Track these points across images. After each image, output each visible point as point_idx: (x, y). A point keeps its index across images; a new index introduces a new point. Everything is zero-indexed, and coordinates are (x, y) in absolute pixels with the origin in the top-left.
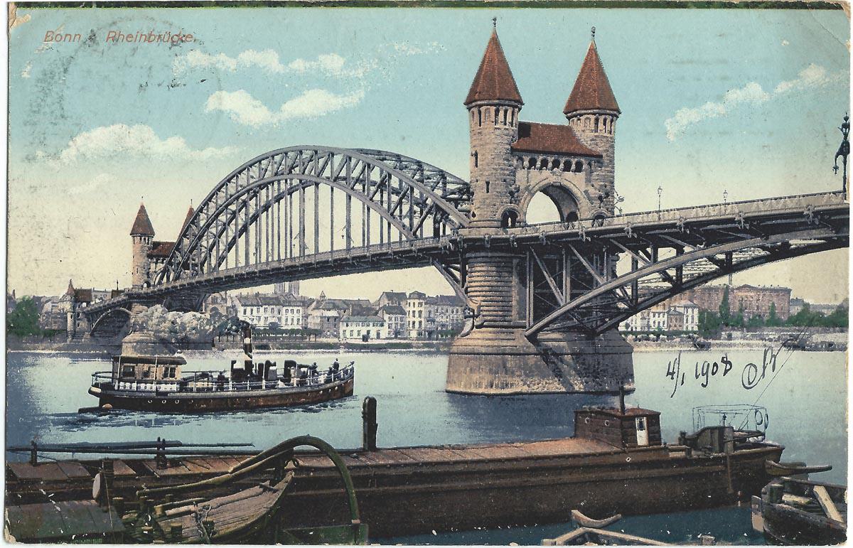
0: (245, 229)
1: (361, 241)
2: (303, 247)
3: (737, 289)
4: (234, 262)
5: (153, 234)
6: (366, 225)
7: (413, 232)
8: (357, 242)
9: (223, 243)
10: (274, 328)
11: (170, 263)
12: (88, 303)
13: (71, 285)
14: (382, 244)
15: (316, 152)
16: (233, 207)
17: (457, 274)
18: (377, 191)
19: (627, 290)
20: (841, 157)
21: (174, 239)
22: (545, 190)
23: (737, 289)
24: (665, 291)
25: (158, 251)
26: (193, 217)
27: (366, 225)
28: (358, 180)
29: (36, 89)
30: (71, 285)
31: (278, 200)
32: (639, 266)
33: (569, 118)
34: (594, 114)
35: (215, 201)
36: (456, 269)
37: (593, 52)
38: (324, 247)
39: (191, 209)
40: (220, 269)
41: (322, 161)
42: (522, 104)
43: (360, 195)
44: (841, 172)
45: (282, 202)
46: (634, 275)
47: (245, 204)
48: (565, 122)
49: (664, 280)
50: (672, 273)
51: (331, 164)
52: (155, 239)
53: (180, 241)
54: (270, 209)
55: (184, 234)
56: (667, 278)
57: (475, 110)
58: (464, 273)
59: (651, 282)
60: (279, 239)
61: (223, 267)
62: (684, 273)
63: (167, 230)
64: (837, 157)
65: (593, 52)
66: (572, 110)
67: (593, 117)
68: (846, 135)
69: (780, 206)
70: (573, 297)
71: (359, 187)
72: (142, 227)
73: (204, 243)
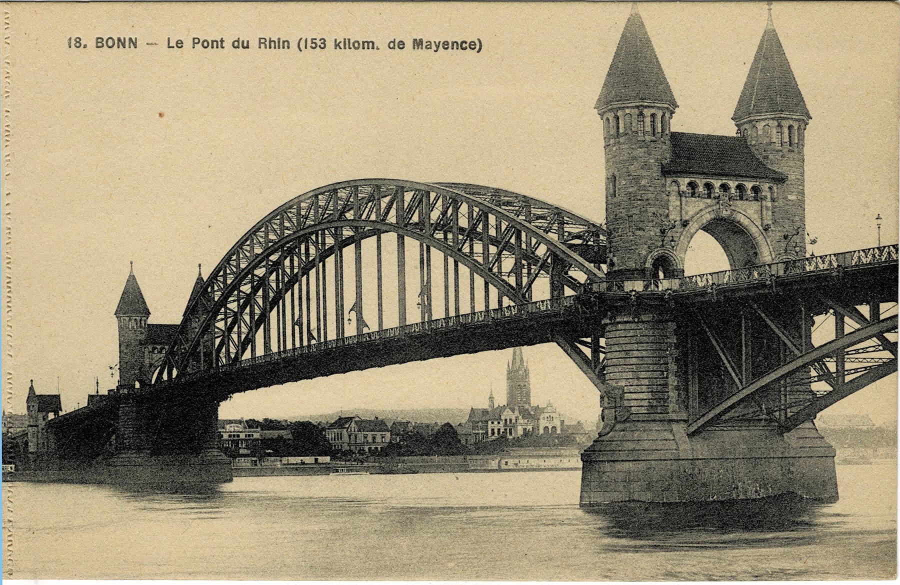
0: (264, 319)
1: (508, 473)
2: (361, 322)
5: (148, 313)
7: (520, 294)
11: (171, 353)
12: (56, 413)
13: (31, 389)
15: (378, 187)
16: (260, 272)
17: (587, 351)
18: (467, 239)
19: (502, 224)
26: (202, 289)
28: (437, 227)
29: (673, 222)
30: (31, 389)
31: (305, 271)
32: (847, 330)
36: (585, 344)
38: (391, 321)
39: (200, 279)
40: (244, 358)
41: (385, 202)
43: (443, 246)
45: (313, 272)
46: (840, 343)
47: (278, 264)
52: (152, 320)
54: (296, 286)
57: (611, 116)
58: (596, 350)
59: (859, 353)
61: (247, 355)
70: (757, 374)
71: (439, 235)
73: (221, 325)
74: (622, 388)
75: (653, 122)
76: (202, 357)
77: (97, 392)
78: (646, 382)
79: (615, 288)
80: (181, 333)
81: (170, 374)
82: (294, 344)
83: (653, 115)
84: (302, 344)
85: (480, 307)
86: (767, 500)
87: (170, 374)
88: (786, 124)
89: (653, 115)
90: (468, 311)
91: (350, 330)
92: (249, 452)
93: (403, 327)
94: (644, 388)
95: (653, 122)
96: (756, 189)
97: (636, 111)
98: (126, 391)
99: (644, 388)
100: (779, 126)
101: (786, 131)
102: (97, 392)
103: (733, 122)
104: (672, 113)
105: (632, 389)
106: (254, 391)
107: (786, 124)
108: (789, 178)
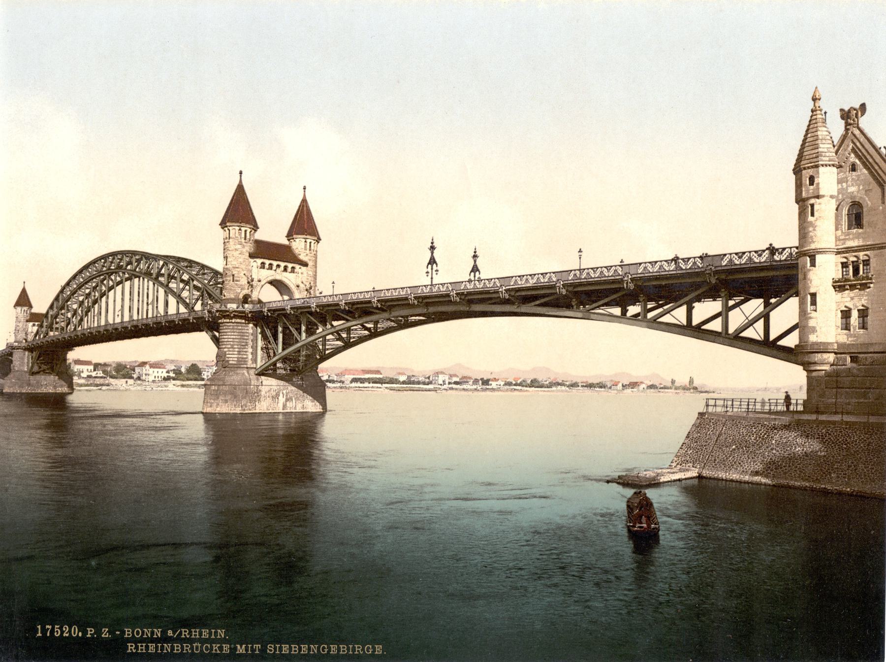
2: (107, 320)
6: (167, 304)
8: (126, 319)
14: (153, 317)
25: (34, 318)
27: (167, 304)
33: (289, 240)
34: (250, 228)
37: (304, 201)
44: (430, 275)
50: (344, 335)
52: (33, 311)
53: (48, 312)
55: (51, 307)
56: (340, 338)
60: (138, 309)
62: (379, 326)
63: (41, 305)
65: (304, 201)
66: (290, 236)
67: (238, 228)
69: (397, 294)
72: (23, 300)
74: (226, 352)
76: (679, 281)
78: (236, 350)
79: (223, 306)
83: (246, 231)
86: (223, 420)
88: (308, 241)
89: (246, 231)
91: (118, 320)
92: (352, 328)
93: (122, 322)
95: (245, 234)
96: (293, 268)
97: (304, 240)
98: (17, 344)
99: (236, 353)
100: (306, 242)
103: (220, 226)
104: (255, 231)
105: (230, 353)
106: (146, 338)
107: (243, 229)
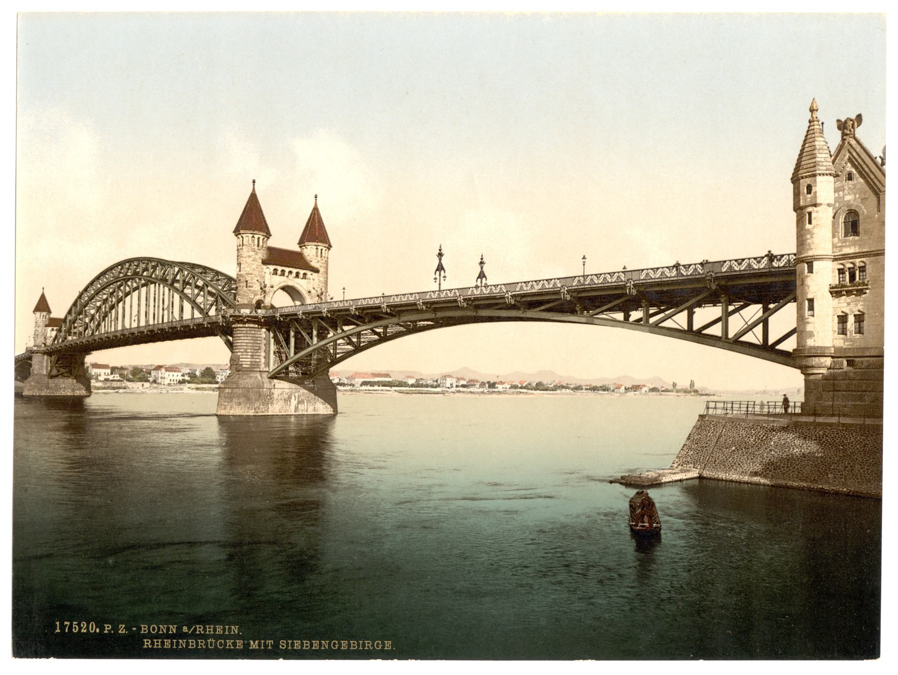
3: (155, 369)
4: (108, 328)
9: (97, 320)
10: (265, 357)
20: (438, 272)
21: (62, 316)
22: (284, 289)
23: (155, 369)
24: (351, 351)
33: (301, 247)
35: (759, 329)
37: (316, 209)
42: (271, 236)
44: (438, 281)
48: (297, 248)
49: (348, 344)
50: (355, 340)
51: (660, 323)
52: (53, 315)
53: (66, 317)
55: (70, 312)
64: (477, 281)
65: (316, 209)
66: (301, 243)
68: (482, 268)
72: (42, 306)
74: (239, 356)
75: (258, 241)
77: (482, 275)
78: (250, 354)
80: (64, 322)
81: (62, 627)
82: (158, 321)
84: (182, 318)
85: (143, 323)
87: (62, 627)
89: (259, 238)
90: (190, 317)
91: (134, 325)
93: (138, 327)
94: (249, 357)
95: (258, 241)
96: (305, 274)
100: (317, 249)
101: (319, 251)
102: (482, 275)
104: (268, 238)
108: (818, 147)
